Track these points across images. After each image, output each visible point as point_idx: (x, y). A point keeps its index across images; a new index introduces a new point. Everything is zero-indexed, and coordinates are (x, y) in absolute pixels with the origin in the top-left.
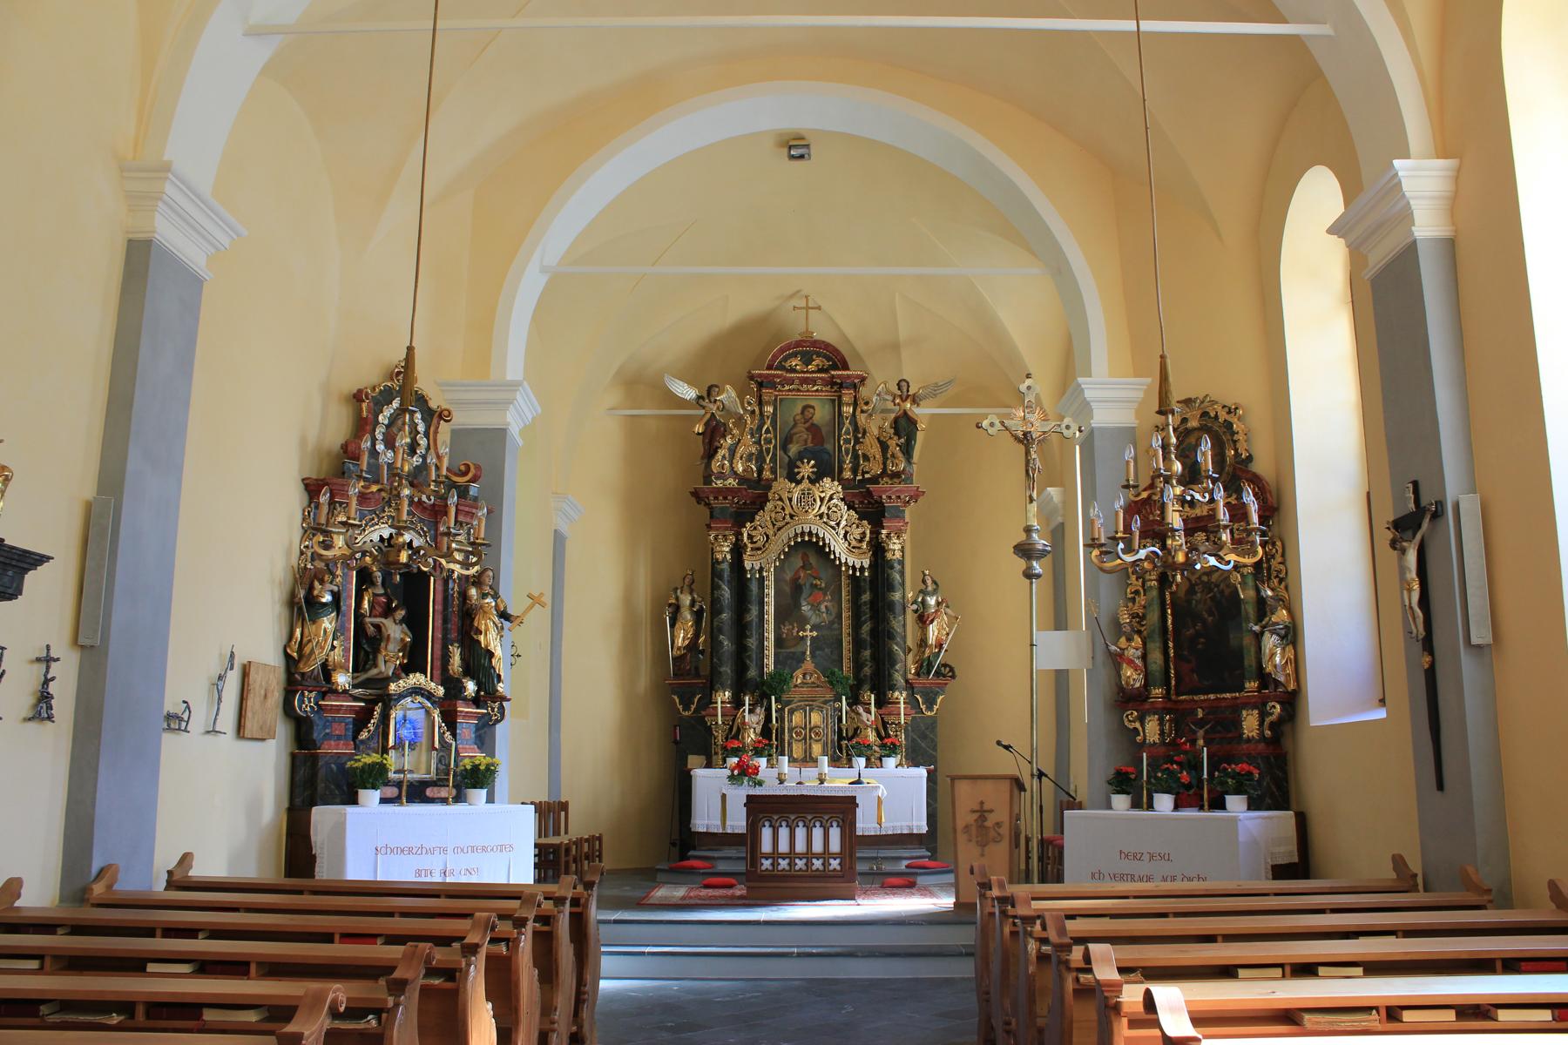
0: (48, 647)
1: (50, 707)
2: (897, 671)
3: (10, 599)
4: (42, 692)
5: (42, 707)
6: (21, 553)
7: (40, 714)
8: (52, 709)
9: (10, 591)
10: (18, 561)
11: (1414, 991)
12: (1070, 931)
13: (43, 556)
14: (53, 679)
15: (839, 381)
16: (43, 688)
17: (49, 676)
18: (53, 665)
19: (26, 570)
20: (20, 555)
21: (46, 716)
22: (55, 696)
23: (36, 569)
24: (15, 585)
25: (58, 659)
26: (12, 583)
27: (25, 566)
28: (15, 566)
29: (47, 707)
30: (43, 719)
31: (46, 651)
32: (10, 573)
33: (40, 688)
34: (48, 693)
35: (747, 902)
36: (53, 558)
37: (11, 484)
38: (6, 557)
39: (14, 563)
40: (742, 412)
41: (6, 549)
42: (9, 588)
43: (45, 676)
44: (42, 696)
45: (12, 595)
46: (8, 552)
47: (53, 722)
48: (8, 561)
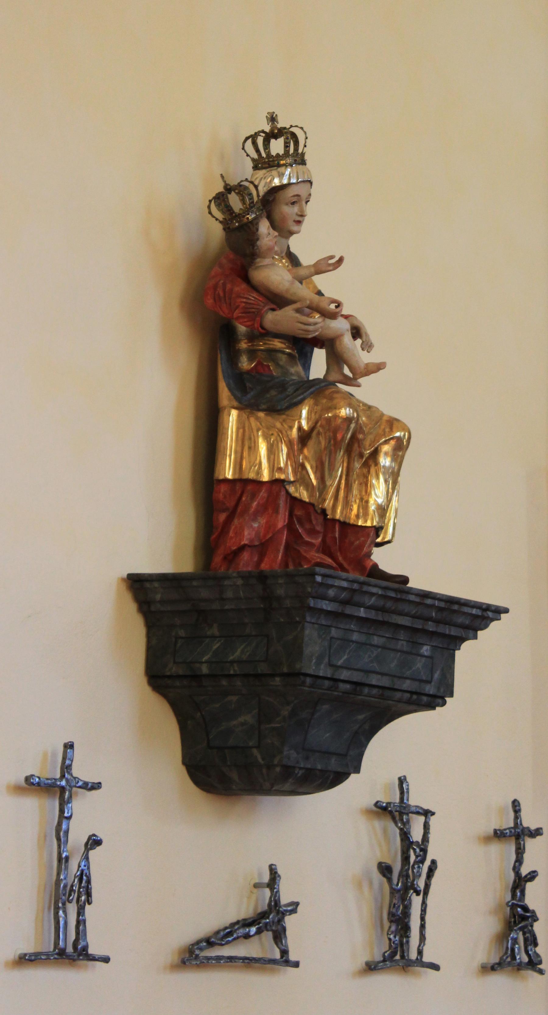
0: (516, 806)
1: (532, 941)
2: (60, 784)
3: (431, 706)
4: (513, 907)
5: (515, 941)
6: (442, 605)
7: (513, 957)
8: (536, 945)
9: (430, 689)
10: (437, 622)
11: (50, 941)
12: (68, 953)
13: (487, 608)
14: (532, 876)
15: (314, 495)
16: (514, 896)
17: (524, 871)
18: (530, 844)
19: (458, 641)
20: (440, 609)
21: (526, 959)
22: (539, 914)
23: (475, 637)
24: (437, 675)
25: (538, 832)
26: (432, 673)
27: (454, 632)
28: (433, 633)
29: (526, 940)
30: (520, 967)
31: (512, 814)
32: (426, 650)
33: (509, 897)
34: (525, 909)
35: (39, 954)
36: (506, 611)
37: (409, 456)
38: (413, 617)
39: (431, 626)
40: (353, 500)
41: (412, 598)
42: (429, 682)
43: (516, 869)
44: (513, 914)
45: (434, 696)
46: (418, 604)
47: (541, 972)
48: (418, 624)
